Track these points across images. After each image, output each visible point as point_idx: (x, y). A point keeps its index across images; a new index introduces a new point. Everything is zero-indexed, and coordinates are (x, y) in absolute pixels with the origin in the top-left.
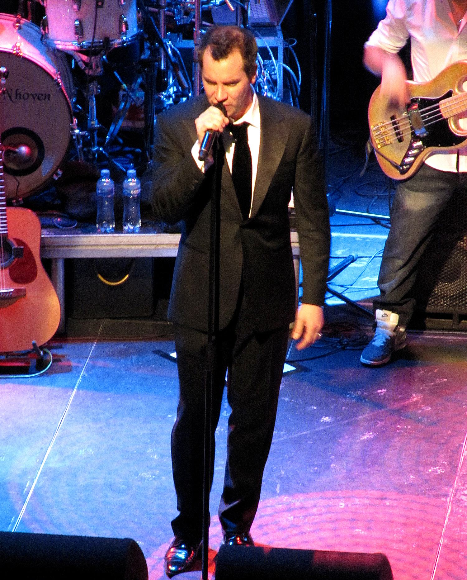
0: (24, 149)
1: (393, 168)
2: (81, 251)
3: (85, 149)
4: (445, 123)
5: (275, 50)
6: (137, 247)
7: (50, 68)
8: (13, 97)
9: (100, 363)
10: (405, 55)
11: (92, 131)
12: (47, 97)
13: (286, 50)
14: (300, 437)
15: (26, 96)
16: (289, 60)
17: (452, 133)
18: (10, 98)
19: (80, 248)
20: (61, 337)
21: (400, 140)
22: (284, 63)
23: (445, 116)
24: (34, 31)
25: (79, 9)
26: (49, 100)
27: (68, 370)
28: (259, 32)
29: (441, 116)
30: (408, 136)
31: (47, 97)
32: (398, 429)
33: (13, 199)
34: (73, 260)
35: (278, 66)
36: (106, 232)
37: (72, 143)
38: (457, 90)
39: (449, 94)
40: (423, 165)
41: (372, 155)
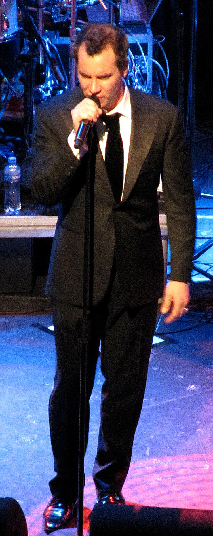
6: (17, 228)
16: (158, 55)
22: (153, 58)
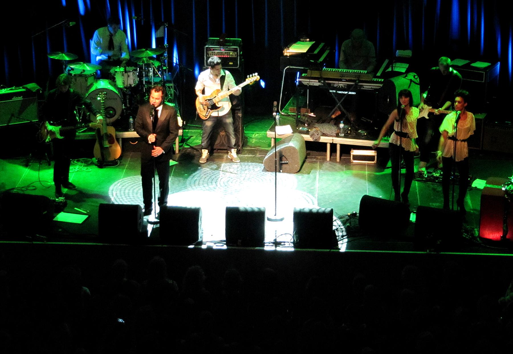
0: (111, 112)
4: (215, 104)
5: (172, 87)
7: (117, 92)
9: (131, 163)
10: (203, 92)
13: (174, 87)
14: (206, 56)
16: (175, 89)
20: (121, 157)
24: (113, 83)
27: (123, 165)
35: (172, 91)
37: (123, 110)
40: (210, 116)
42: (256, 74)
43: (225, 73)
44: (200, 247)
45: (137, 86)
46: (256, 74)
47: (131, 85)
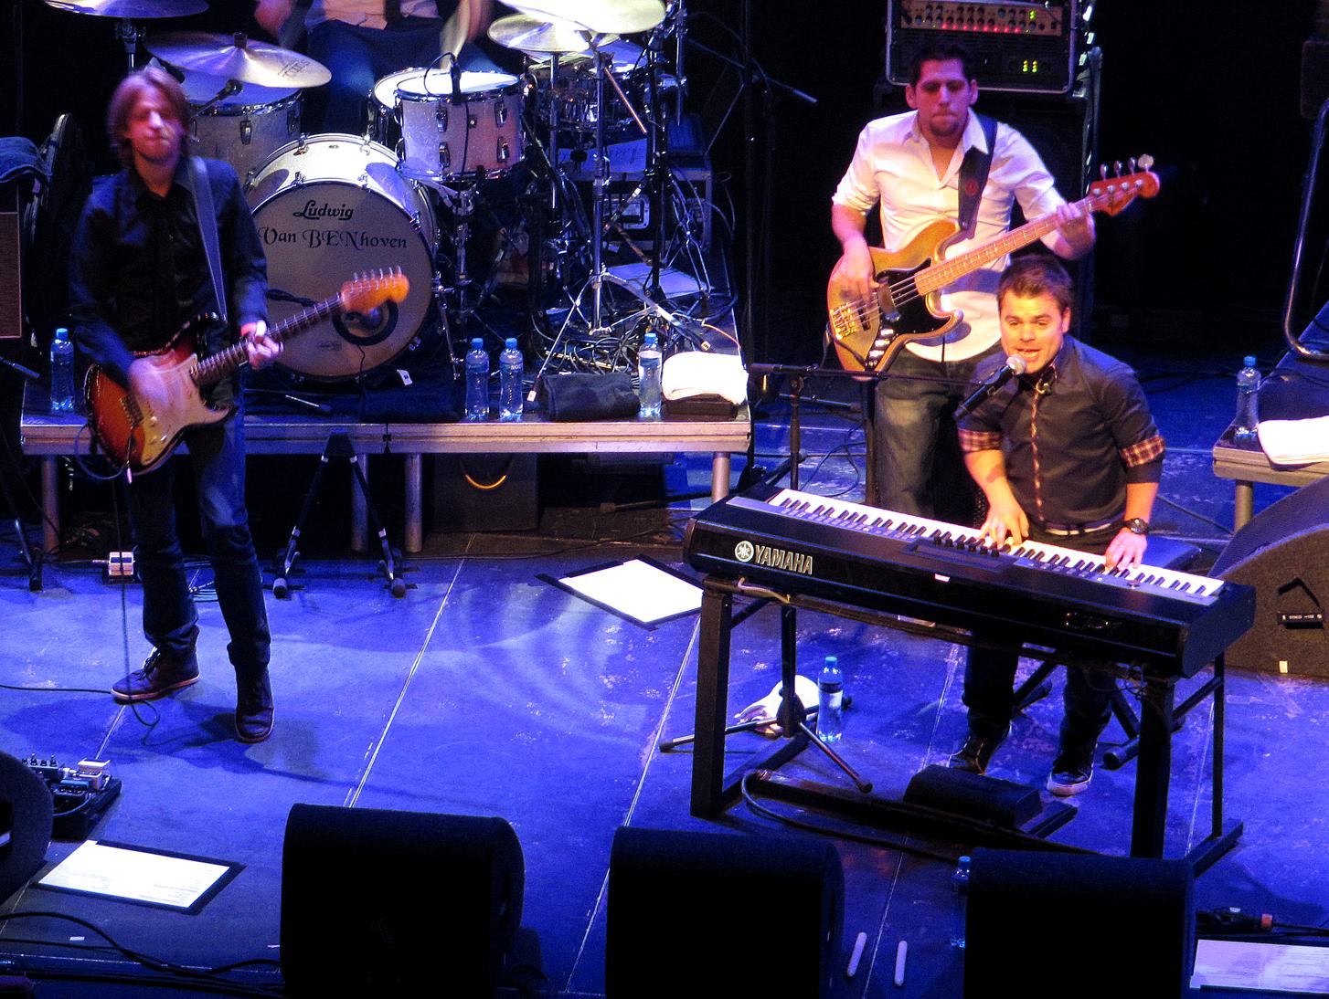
1: (856, 361)
2: (444, 444)
3: (452, 311)
5: (701, 185)
6: (517, 440)
8: (358, 242)
10: (873, 231)
11: (459, 288)
12: (402, 243)
15: (374, 242)
16: (718, 198)
17: (930, 316)
18: (354, 244)
19: (442, 440)
21: (866, 327)
22: (713, 202)
23: (921, 293)
25: (445, 127)
26: (405, 246)
28: (738, 301)
29: (916, 293)
30: (875, 322)
31: (402, 243)
32: (855, 679)
33: (357, 375)
34: (433, 455)
36: (477, 420)
38: (936, 258)
39: (927, 264)
41: (832, 347)
42: (1147, 162)
43: (991, 141)
44: (497, 644)
45: (518, 176)
46: (1147, 162)
47: (481, 170)
